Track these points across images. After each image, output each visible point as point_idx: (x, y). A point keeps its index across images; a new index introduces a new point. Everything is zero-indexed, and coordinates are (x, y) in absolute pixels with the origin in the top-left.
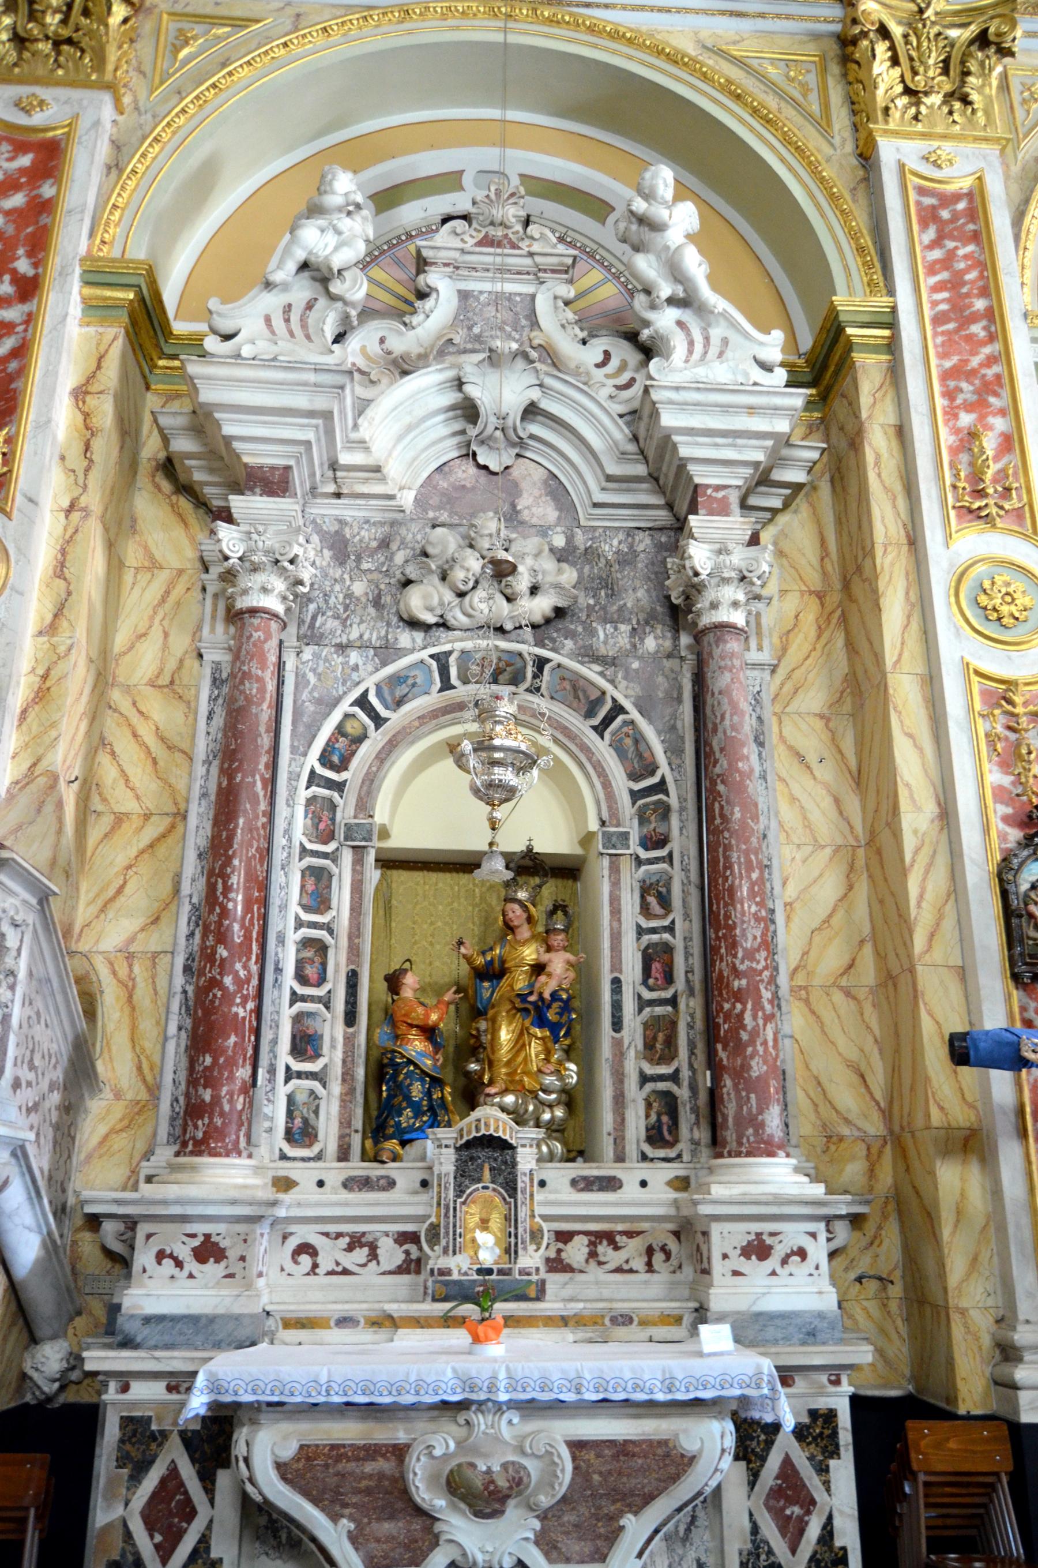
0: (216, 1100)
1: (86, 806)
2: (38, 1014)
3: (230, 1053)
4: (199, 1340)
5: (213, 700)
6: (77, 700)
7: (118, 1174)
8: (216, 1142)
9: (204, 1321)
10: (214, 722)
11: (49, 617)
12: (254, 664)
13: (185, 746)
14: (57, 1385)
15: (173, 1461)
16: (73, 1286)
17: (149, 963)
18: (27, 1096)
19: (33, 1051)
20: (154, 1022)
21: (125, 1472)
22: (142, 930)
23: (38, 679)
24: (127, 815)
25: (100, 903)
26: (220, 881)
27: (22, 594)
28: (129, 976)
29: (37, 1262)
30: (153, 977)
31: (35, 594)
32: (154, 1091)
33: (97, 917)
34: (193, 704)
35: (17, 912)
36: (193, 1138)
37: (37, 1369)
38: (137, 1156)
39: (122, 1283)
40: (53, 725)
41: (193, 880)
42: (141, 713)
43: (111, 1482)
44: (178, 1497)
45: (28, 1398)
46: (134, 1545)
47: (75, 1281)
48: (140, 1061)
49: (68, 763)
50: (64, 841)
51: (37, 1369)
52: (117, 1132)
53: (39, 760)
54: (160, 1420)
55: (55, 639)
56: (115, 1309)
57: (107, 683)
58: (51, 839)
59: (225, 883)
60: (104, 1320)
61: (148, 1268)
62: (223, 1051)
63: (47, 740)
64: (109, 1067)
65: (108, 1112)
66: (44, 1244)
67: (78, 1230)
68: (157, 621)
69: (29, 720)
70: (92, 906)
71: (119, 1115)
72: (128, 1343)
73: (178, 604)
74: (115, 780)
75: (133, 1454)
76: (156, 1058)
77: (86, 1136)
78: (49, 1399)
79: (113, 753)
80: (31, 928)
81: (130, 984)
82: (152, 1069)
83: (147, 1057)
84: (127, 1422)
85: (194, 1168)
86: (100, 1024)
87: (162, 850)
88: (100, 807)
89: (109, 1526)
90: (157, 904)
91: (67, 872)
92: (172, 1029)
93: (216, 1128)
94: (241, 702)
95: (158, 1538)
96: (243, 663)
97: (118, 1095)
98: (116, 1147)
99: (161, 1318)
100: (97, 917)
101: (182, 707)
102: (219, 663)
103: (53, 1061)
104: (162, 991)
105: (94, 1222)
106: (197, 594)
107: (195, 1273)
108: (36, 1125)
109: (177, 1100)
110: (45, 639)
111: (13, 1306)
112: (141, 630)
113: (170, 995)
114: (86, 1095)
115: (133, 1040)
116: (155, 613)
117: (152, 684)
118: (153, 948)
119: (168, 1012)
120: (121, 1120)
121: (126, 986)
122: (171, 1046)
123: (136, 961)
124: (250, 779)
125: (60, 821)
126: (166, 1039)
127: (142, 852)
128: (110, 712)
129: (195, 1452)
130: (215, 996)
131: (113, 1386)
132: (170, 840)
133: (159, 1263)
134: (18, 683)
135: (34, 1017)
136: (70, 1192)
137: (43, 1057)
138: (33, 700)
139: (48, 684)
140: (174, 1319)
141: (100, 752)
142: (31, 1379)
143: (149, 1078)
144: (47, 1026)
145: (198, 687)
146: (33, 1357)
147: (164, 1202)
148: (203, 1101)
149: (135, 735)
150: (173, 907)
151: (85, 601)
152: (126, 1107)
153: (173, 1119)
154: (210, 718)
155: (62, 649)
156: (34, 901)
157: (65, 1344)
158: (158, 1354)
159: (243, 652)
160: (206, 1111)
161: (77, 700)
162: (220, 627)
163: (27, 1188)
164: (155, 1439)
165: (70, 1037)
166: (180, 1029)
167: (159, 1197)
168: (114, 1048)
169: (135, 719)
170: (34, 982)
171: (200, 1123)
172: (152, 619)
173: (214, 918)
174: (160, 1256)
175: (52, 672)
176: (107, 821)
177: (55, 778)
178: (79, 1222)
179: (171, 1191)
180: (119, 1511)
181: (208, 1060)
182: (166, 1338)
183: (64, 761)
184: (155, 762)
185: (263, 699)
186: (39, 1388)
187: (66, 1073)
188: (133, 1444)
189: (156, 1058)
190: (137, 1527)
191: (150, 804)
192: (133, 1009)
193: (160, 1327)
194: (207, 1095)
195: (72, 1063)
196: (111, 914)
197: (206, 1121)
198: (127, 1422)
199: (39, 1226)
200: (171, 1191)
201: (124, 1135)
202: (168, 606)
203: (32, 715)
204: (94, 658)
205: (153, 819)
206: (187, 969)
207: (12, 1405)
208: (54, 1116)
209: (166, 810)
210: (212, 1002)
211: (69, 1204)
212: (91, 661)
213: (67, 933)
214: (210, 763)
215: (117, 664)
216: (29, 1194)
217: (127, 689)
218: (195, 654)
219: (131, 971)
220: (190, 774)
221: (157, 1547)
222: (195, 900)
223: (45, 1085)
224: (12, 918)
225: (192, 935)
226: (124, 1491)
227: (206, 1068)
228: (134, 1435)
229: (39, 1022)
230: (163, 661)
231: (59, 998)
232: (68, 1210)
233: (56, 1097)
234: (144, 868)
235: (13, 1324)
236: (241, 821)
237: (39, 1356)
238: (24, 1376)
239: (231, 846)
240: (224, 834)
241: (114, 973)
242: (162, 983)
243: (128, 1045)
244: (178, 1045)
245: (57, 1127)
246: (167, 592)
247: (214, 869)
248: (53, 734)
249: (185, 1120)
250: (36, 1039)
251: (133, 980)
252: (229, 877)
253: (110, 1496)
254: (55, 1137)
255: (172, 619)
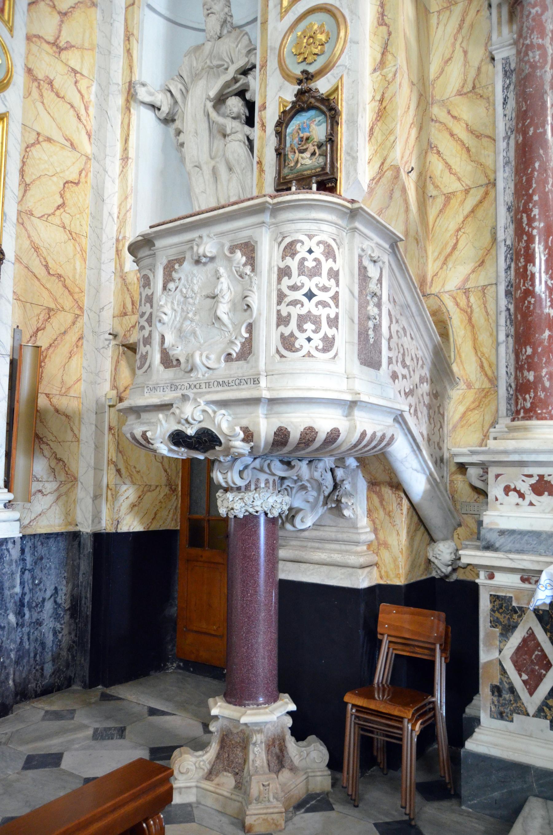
0: (538, 379)
1: (424, 192)
2: (404, 329)
3: (546, 343)
4: (541, 548)
5: (506, 88)
6: (406, 112)
7: (475, 437)
8: (542, 410)
9: (544, 536)
10: (508, 106)
11: (379, 56)
12: (535, 36)
13: (488, 132)
14: (450, 569)
15: (530, 628)
16: (452, 509)
17: (480, 294)
18: (406, 385)
19: (404, 355)
20: (488, 334)
21: (497, 631)
22: (473, 271)
23: (377, 103)
24: (453, 193)
25: (442, 258)
26: (524, 215)
27: (358, 43)
28: (468, 304)
29: (425, 492)
30: (485, 303)
31: (368, 44)
32: (493, 381)
33: (441, 268)
34: (491, 99)
35: (373, 251)
36: (524, 408)
37: (436, 558)
38: (487, 426)
39: (485, 507)
40: (391, 132)
41: (506, 228)
42: (454, 117)
43: (487, 635)
44: (536, 653)
45: (434, 574)
46: (508, 678)
47: (455, 505)
48: (482, 362)
49: (405, 159)
50: (411, 217)
51: (436, 558)
52: (471, 410)
53: (385, 160)
54: (518, 600)
55: (385, 70)
56: (480, 523)
57: (428, 102)
58: (402, 217)
59: (529, 217)
60: (476, 531)
61: (498, 497)
62: (541, 343)
63: (388, 144)
64: (461, 367)
65: (464, 397)
66: (428, 480)
67: (453, 474)
68: (458, 46)
69: (375, 134)
70: (437, 262)
71: (472, 399)
72: (489, 547)
73: (472, 26)
74: (442, 171)
75: (502, 620)
76: (493, 359)
77: (451, 414)
78: (447, 576)
79: (438, 152)
80: (387, 263)
81: (469, 310)
82: (490, 366)
83: (486, 359)
84: (495, 598)
85: (526, 429)
86: (451, 340)
87: (480, 213)
88: (434, 193)
89: (490, 663)
90: (481, 252)
91: (417, 240)
92: (502, 337)
93: (540, 400)
94: (527, 70)
95: (525, 677)
96: (526, 38)
97: (469, 386)
98: (472, 420)
99: (512, 532)
100: (441, 268)
101: (483, 103)
102: (508, 58)
103: (420, 362)
104: (492, 312)
105: (462, 467)
106: (485, 12)
107: (534, 502)
108: (413, 404)
109: (511, 386)
110: (378, 73)
111: (416, 519)
112: (447, 56)
113: (498, 313)
114: (448, 387)
115: (475, 349)
116: (456, 40)
117: (460, 93)
118: (482, 282)
119: (497, 326)
120: (473, 402)
121: (466, 312)
122: (502, 349)
123: (471, 294)
124: (541, 130)
125: (406, 201)
126: (498, 344)
127: (467, 217)
128: (433, 124)
129: (547, 625)
130: (529, 302)
131: (482, 574)
132: (486, 204)
133: (507, 495)
134: (364, 109)
135: (401, 332)
136: (445, 450)
137: (412, 359)
138: (376, 119)
139: (384, 104)
140: (522, 533)
141: (429, 154)
142: (434, 563)
143: (489, 373)
144: (412, 338)
145: (493, 85)
146: (433, 550)
147: (505, 452)
148: (528, 380)
149: (452, 135)
150: (493, 252)
151: (401, 35)
152: (476, 394)
153: (509, 399)
154: (505, 103)
155: (390, 76)
156: (387, 246)
157: (452, 544)
158: (511, 556)
159: (525, 29)
160: (531, 388)
161: (406, 112)
162: (505, 30)
163: (411, 444)
164: (516, 612)
165: (430, 347)
166: (507, 336)
167: (501, 448)
168: (463, 355)
169: (451, 123)
170: (398, 307)
171: (527, 396)
172: (454, 45)
173: (523, 244)
174: (507, 490)
175: (386, 95)
176: (440, 201)
177: (397, 170)
178: (453, 468)
179: (511, 445)
180: (495, 655)
181: (529, 351)
182: (517, 546)
183: (402, 157)
184: (468, 150)
185: (546, 62)
186: (439, 569)
187: (431, 371)
188: (501, 613)
189: (493, 359)
190: (509, 667)
191: (468, 182)
192: (473, 327)
193: (512, 538)
194: (531, 376)
195: (434, 364)
196: (450, 265)
197: (532, 395)
198: (495, 598)
199: (423, 469)
200: (511, 445)
201: (476, 412)
202: (464, 31)
203: (376, 130)
204: (415, 81)
205: (472, 191)
206: (508, 293)
207: (424, 577)
208: (427, 399)
209: (480, 182)
210: (528, 307)
211: (445, 457)
212: (413, 84)
213: (423, 282)
214: (509, 138)
215: (434, 88)
216: (412, 447)
217: (443, 103)
218: (489, 59)
219: (469, 301)
220: (495, 152)
221: (524, 682)
222: (509, 242)
223: (416, 379)
224: (370, 256)
225: (509, 267)
226: (498, 643)
227: (528, 357)
228: (501, 607)
229: (405, 335)
230: (465, 74)
231: (418, 319)
232: (445, 461)
233: (425, 387)
234: (469, 229)
235: (416, 530)
236: (537, 165)
237: (436, 549)
238: (429, 561)
239: (531, 186)
240: (524, 178)
241: (457, 304)
242: (491, 306)
243: (472, 353)
244: (507, 348)
245: (429, 407)
246: (463, 21)
247: (519, 207)
248: (392, 138)
249: (517, 396)
250: (405, 347)
251: (471, 307)
252: (531, 210)
253: (489, 645)
254: (429, 414)
255: (468, 40)
